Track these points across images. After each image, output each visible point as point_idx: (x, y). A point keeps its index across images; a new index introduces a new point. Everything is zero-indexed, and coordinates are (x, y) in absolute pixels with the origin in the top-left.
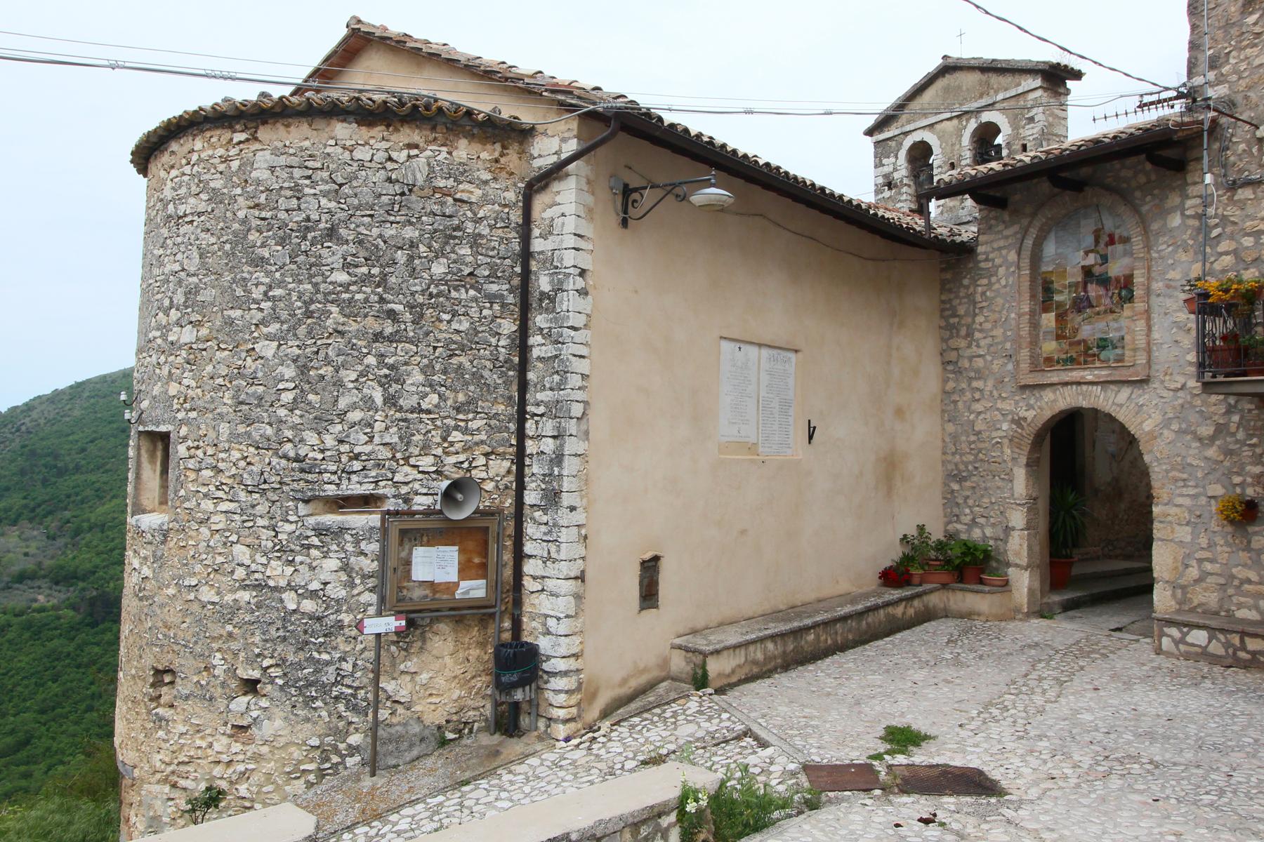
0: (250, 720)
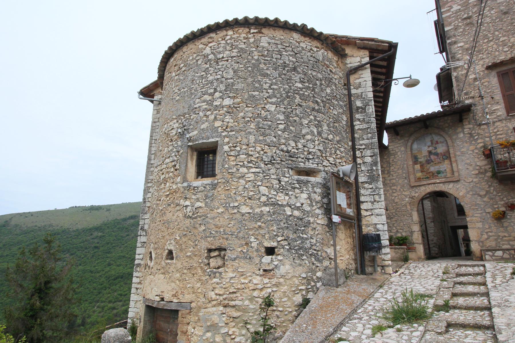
0: (273, 266)
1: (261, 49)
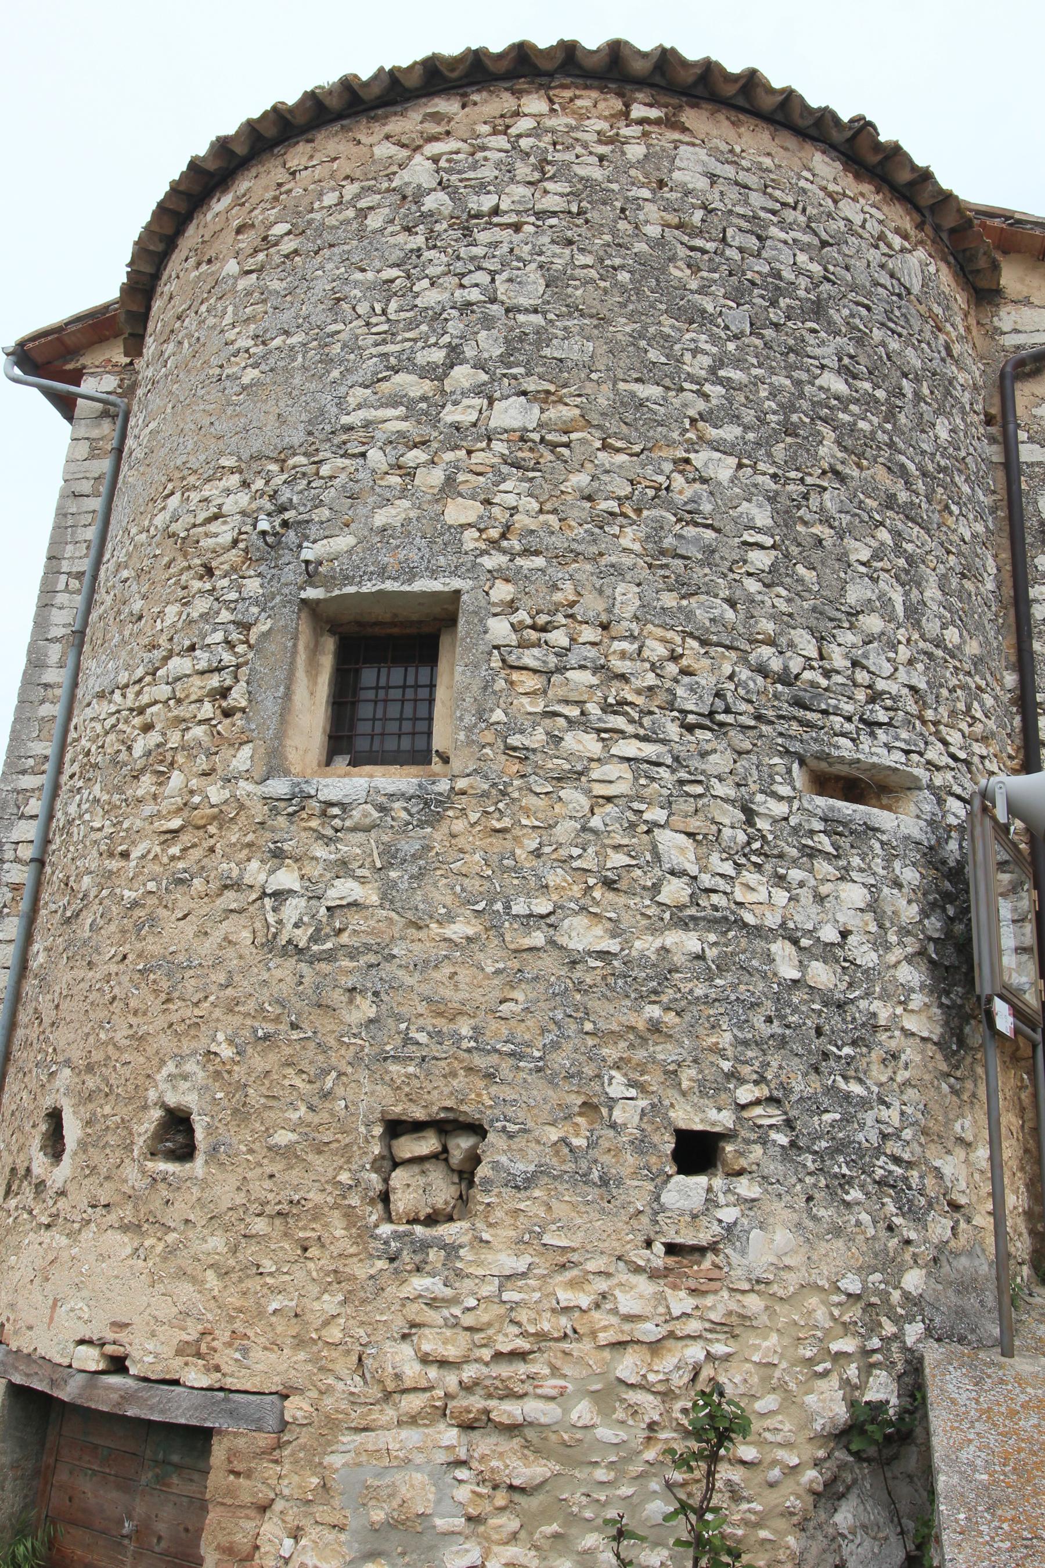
0: (716, 1229)
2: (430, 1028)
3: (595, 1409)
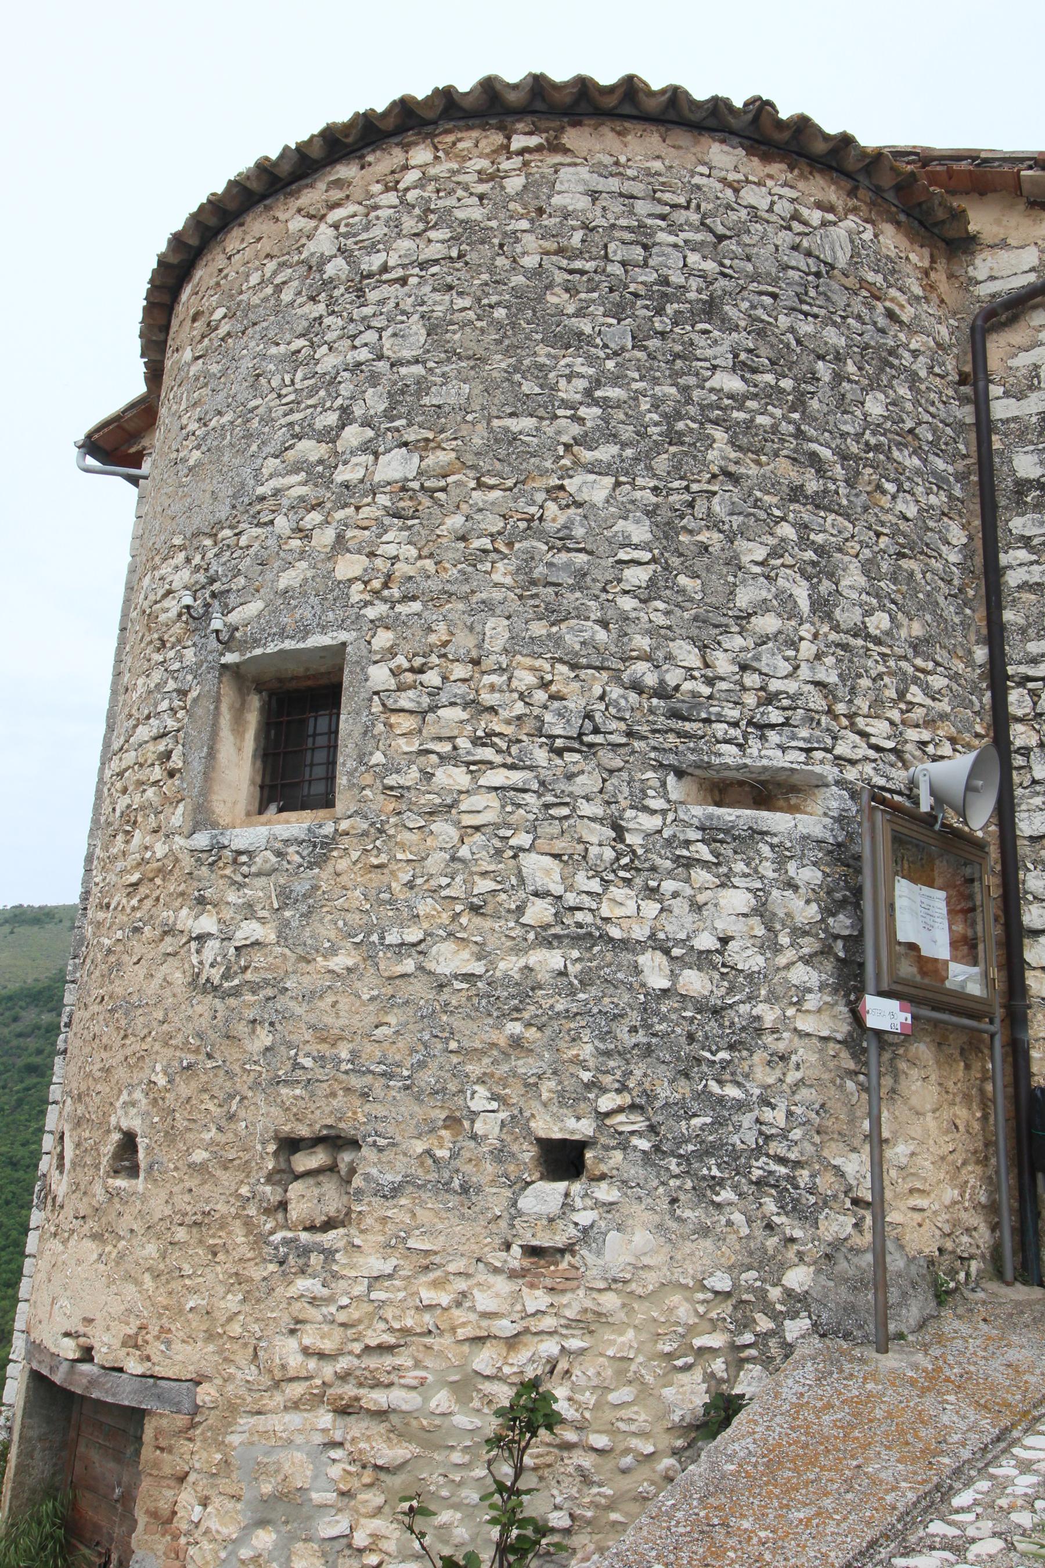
0: (572, 1231)
1: (553, 220)
2: (315, 1054)
3: (453, 1399)
